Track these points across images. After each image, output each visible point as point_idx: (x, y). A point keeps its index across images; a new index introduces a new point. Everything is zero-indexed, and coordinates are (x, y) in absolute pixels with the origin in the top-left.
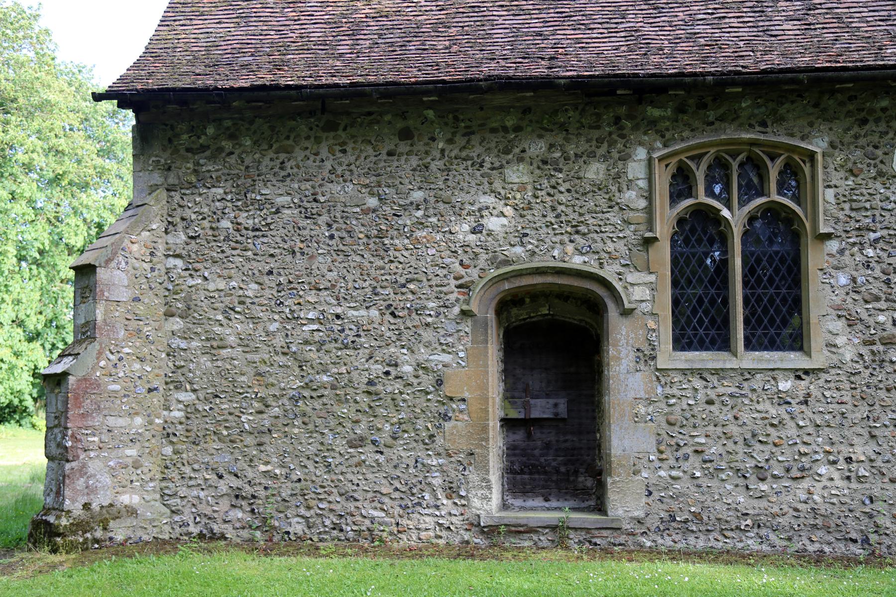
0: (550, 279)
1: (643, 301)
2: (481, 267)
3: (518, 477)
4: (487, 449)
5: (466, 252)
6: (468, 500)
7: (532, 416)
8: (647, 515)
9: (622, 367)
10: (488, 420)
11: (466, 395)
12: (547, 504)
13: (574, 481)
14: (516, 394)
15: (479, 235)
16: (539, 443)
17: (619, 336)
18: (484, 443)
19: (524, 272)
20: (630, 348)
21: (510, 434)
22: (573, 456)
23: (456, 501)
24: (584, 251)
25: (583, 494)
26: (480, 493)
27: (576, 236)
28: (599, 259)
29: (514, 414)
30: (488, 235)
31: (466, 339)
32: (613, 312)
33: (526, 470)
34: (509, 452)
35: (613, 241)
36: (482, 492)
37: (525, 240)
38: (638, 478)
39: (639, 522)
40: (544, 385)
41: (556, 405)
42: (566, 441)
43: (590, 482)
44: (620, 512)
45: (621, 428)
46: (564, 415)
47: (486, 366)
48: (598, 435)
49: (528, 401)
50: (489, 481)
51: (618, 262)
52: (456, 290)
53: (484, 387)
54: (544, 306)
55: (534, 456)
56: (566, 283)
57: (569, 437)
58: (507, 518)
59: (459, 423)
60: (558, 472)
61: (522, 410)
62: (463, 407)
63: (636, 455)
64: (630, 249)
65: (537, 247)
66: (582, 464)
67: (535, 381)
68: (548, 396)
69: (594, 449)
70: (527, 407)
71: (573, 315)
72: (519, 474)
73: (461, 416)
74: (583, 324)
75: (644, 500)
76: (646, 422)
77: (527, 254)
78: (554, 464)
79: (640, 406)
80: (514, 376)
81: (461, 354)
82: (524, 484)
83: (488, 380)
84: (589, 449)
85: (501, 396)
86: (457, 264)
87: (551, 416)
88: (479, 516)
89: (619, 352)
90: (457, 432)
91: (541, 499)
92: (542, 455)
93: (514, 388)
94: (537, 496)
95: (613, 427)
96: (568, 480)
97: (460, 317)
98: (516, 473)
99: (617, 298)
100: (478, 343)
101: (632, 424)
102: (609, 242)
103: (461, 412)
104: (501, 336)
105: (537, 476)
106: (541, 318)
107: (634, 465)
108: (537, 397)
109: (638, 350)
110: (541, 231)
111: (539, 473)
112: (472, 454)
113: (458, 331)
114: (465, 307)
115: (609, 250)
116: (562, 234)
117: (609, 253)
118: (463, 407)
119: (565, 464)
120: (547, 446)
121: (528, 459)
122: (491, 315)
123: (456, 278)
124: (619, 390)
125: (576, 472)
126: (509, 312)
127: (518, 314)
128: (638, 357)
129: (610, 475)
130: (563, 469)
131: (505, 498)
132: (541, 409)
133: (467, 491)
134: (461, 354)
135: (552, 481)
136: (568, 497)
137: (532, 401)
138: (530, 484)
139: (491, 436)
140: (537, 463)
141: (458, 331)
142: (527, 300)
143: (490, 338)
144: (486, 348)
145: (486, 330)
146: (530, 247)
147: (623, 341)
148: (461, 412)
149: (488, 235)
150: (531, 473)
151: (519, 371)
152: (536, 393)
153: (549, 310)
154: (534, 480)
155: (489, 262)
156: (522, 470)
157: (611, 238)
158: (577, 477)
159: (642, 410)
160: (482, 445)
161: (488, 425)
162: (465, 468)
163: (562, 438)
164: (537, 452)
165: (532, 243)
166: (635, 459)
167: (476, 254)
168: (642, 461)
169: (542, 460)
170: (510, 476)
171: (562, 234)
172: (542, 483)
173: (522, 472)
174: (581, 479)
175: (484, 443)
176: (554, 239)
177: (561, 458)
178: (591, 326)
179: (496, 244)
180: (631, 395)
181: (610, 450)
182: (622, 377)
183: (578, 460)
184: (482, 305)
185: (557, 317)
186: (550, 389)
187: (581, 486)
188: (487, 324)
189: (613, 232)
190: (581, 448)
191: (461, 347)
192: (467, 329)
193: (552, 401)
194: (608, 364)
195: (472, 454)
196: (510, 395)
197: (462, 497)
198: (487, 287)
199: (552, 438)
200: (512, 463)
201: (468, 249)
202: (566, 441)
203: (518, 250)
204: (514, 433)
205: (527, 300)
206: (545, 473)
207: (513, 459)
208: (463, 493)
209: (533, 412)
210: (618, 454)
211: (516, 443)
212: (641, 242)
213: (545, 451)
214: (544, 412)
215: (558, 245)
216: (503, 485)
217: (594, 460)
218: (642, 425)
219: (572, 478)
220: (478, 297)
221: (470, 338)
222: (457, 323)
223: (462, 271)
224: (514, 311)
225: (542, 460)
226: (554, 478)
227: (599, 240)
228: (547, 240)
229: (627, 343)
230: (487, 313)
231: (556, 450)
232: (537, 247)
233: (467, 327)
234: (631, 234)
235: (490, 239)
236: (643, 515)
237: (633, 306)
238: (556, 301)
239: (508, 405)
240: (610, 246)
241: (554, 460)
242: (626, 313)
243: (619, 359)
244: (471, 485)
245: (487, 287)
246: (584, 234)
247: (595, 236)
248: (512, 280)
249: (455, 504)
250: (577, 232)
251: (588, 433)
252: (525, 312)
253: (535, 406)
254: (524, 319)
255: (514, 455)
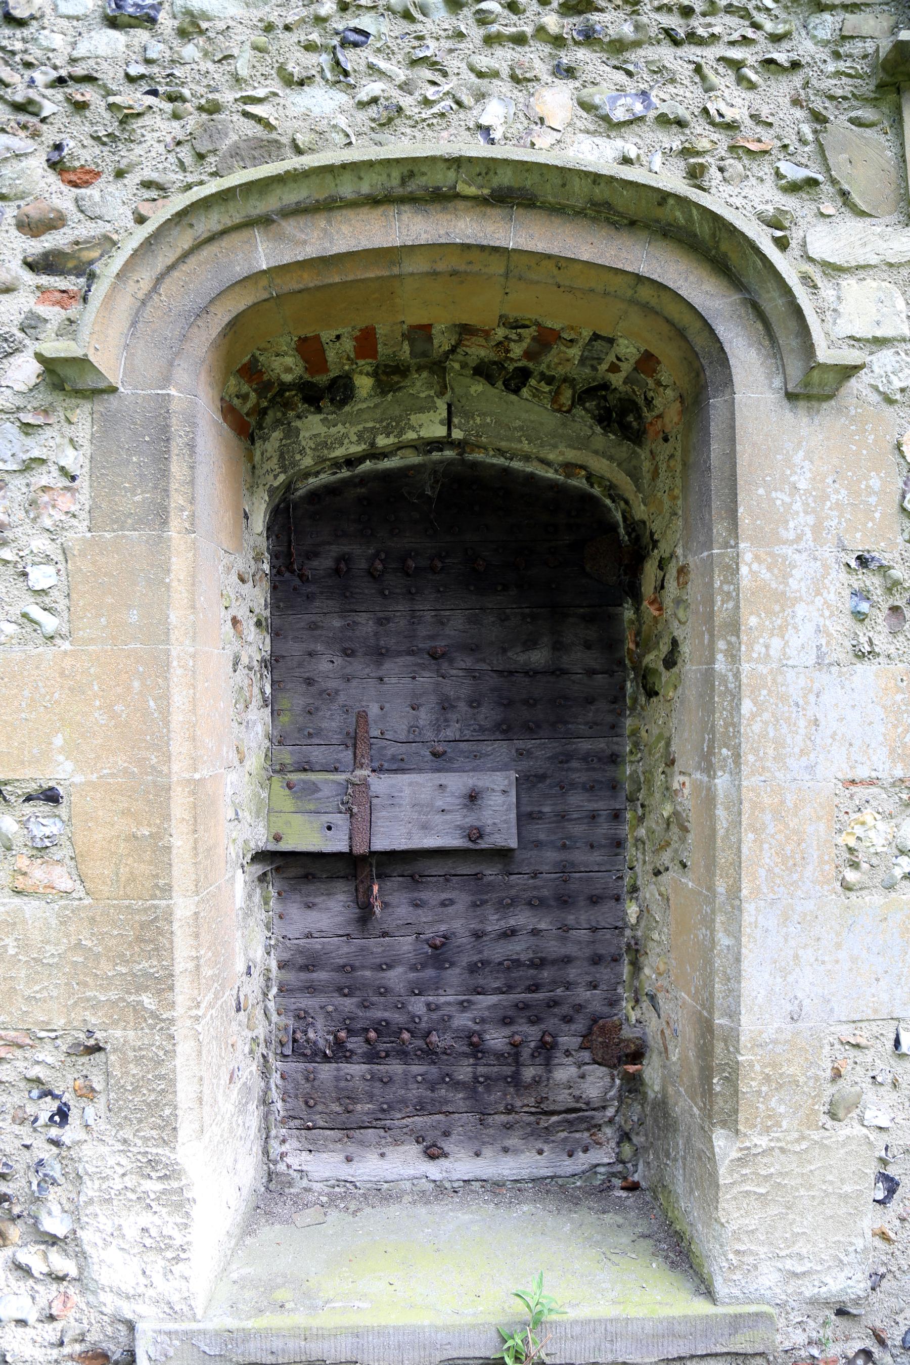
0: (465, 228)
1: (880, 342)
2: (148, 174)
3: (326, 1071)
4: (163, 1024)
5: (80, 107)
6: (81, 1256)
7: (380, 844)
8: (877, 1279)
9: (795, 641)
10: (167, 890)
11: (61, 772)
12: (434, 1170)
13: (537, 1081)
14: (317, 754)
15: (141, 35)
16: (406, 944)
17: (781, 497)
18: (148, 1001)
19: (347, 189)
20: (828, 553)
21: (294, 910)
22: (535, 988)
23: (24, 1257)
24: (619, 115)
25: (570, 1125)
26: (133, 1222)
27: (582, 54)
28: (686, 152)
29: (306, 836)
30: (182, 33)
31: (65, 502)
32: (752, 380)
33: (355, 1044)
34: (291, 977)
35: (741, 79)
36: (146, 1219)
37: (350, 59)
38: (849, 1129)
39: (841, 1312)
40: (424, 716)
41: (473, 798)
42: (509, 934)
43: (597, 1083)
44: (768, 1280)
45: (785, 918)
46: (505, 836)
47: (158, 631)
48: (632, 910)
49: (365, 784)
50: (171, 1173)
51: (766, 170)
52: (29, 278)
53: (146, 736)
54: (427, 407)
55: (384, 991)
56: (540, 246)
57: (522, 919)
58: (260, 1334)
59: (30, 907)
60: (476, 1048)
61: (340, 820)
62: (53, 827)
63: (846, 1033)
64: (818, 118)
65: (406, 87)
66: (568, 1020)
67: (394, 700)
68: (440, 760)
69: (616, 959)
70: (356, 805)
71: (535, 439)
72: (326, 1059)
73: (39, 873)
74: (579, 482)
75: (872, 1220)
76: (890, 887)
77: (362, 116)
78: (462, 1020)
79: (868, 815)
80: (309, 682)
81: (41, 577)
82: (347, 1098)
83: (165, 698)
84: (596, 960)
85: (255, 761)
86: (37, 164)
87: (454, 841)
88: (131, 1327)
89: (784, 571)
90: (24, 945)
91: (414, 1149)
92: (417, 990)
93: (309, 734)
94: (397, 1142)
95: (750, 911)
96: (515, 1081)
97: (44, 397)
98: (317, 1055)
99: (779, 320)
100: (118, 522)
101: (834, 898)
102: (724, 80)
103: (41, 851)
104: (259, 523)
105: (396, 1068)
106: (414, 459)
107: (837, 1075)
108: (399, 766)
109: (863, 561)
110: (426, 26)
111: (403, 1055)
112: (97, 1049)
113: (31, 465)
114: (54, 348)
115: (730, 114)
116: (519, 40)
117: (732, 127)
118: (53, 827)
119: (506, 1021)
120: (438, 953)
121: (365, 1005)
122: (193, 399)
123: (30, 227)
124: (779, 744)
125: (546, 1050)
126: (291, 433)
127: (326, 440)
128: (862, 594)
129: (730, 1122)
130: (496, 1039)
131: (276, 1148)
132: (414, 811)
133: (74, 1212)
134: (41, 577)
135: (457, 1085)
136: (513, 1141)
137: (380, 784)
138: (371, 1097)
139: (182, 961)
140: (398, 1018)
141: (31, 465)
142: (364, 384)
143: (177, 499)
144: (160, 545)
145: (162, 459)
146: (373, 88)
147: (801, 521)
148: (41, 851)
149: (182, 33)
150: (372, 1057)
151: (327, 665)
152: (393, 750)
153: (449, 424)
154: (387, 1081)
155: (185, 153)
156: (339, 1044)
157: (736, 65)
158: (548, 1064)
159: (877, 835)
160: (138, 1009)
161: (168, 916)
162: (63, 1115)
163: (494, 923)
164: (396, 977)
165: (383, 71)
166: (840, 1052)
167: (127, 117)
168: (867, 1057)
169: (418, 1006)
170: (296, 1067)
171: (519, 40)
172: (415, 1092)
173: (339, 1052)
174: (564, 1073)
175: (148, 1001)
176: (483, 62)
177: (493, 999)
178: (612, 490)
179: (219, 74)
180: (835, 765)
181: (734, 1015)
182: (794, 683)
183: (554, 1003)
184: (161, 360)
185: (478, 456)
186: (450, 733)
187: (563, 1098)
188: (164, 436)
189: (745, 41)
190: (567, 960)
191: (40, 543)
192: (70, 459)
193: (457, 783)
194: (734, 626)
195: (97, 1049)
196: (293, 759)
197: (53, 1240)
198: (165, 257)
199: (457, 922)
200: (301, 1016)
201: (89, 94)
202: (509, 934)
203: (323, 102)
204: (309, 906)
205: (364, 384)
206: (429, 1054)
207: (307, 1002)
208: (55, 1224)
209: (381, 817)
210: (770, 1032)
211: (316, 944)
212: (867, 88)
213: (430, 973)
214: (425, 827)
215: (503, 86)
216: (265, 1102)
217: (613, 1002)
218: (875, 899)
219: (529, 1073)
220: (125, 304)
221: (84, 495)
222: (27, 428)
223: (58, 196)
224: (312, 426)
225: (418, 1006)
226: (464, 1072)
227: (685, 71)
228: (452, 64)
229: (817, 529)
230: (166, 380)
231: (473, 969)
232: (406, 87)
233: (70, 439)
234: (823, 54)
235: (190, 51)
236: (859, 1286)
237: (851, 356)
238: (478, 387)
239: (284, 800)
240: (733, 103)
241: (464, 1006)
242: (815, 386)
243: (783, 600)
244: (90, 1189)
245: (165, 257)
246: (619, 46)
247: (666, 54)
248: (290, 227)
249: (24, 1270)
250: (589, 38)
251: (594, 900)
252: (353, 431)
253: (393, 801)
254: (350, 462)
255: (311, 989)
